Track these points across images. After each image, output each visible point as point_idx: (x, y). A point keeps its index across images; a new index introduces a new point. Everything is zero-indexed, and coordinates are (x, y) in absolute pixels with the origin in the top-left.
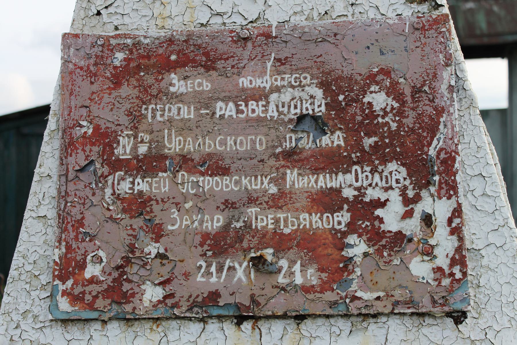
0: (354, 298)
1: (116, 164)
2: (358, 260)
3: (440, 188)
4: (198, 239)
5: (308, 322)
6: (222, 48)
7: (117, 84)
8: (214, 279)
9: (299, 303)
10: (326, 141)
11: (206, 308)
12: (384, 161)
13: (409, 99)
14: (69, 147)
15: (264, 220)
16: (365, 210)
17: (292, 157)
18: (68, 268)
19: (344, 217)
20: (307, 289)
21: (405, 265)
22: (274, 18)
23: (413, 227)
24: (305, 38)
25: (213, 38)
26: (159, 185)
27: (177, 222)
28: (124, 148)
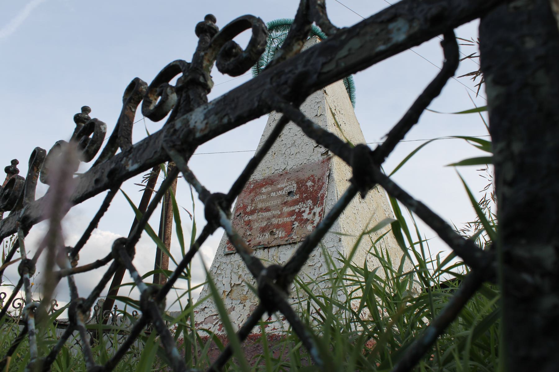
5: (281, 247)
6: (276, 179)
7: (250, 193)
10: (294, 197)
15: (275, 221)
17: (285, 204)
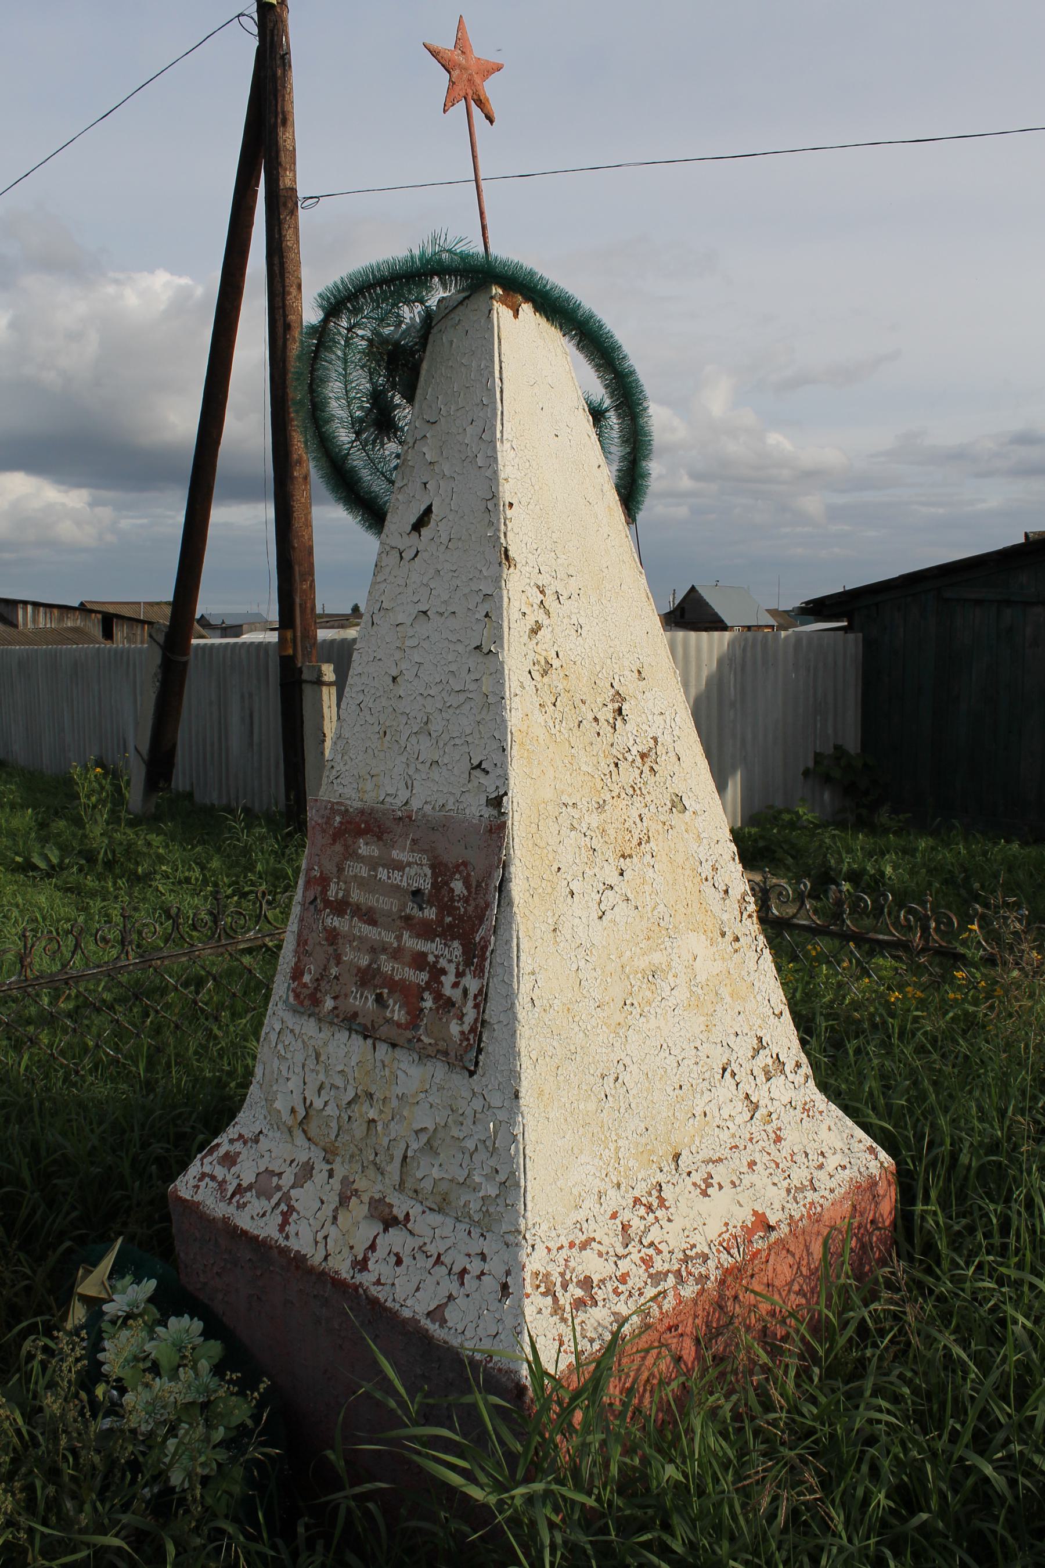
0: (419, 1040)
2: (426, 1011)
3: (476, 969)
4: (355, 971)
8: (357, 1003)
12: (453, 939)
13: (473, 890)
14: (308, 883)
20: (399, 1025)
21: (448, 1023)
25: (384, 814)
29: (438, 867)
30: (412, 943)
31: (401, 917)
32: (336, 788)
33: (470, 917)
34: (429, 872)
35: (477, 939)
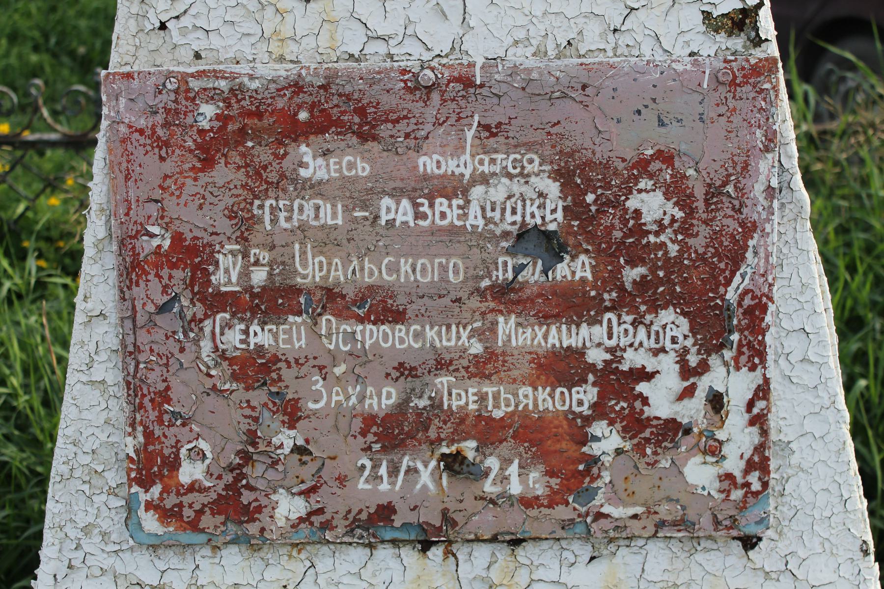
1: (217, 301)
2: (607, 460)
3: (740, 353)
4: (358, 424)
8: (384, 486)
9: (514, 520)
11: (374, 525)
12: (654, 308)
14: (132, 270)
15: (462, 397)
16: (620, 384)
17: (506, 296)
18: (151, 466)
19: (586, 395)
20: (527, 502)
22: (478, 51)
23: (693, 412)
24: (531, 89)
25: (372, 83)
26: (287, 336)
27: (322, 397)
28: (227, 273)
29: (572, 174)
30: (516, 334)
31: (482, 294)
32: (176, 38)
33: (702, 258)
34: (553, 188)
35: (731, 295)
